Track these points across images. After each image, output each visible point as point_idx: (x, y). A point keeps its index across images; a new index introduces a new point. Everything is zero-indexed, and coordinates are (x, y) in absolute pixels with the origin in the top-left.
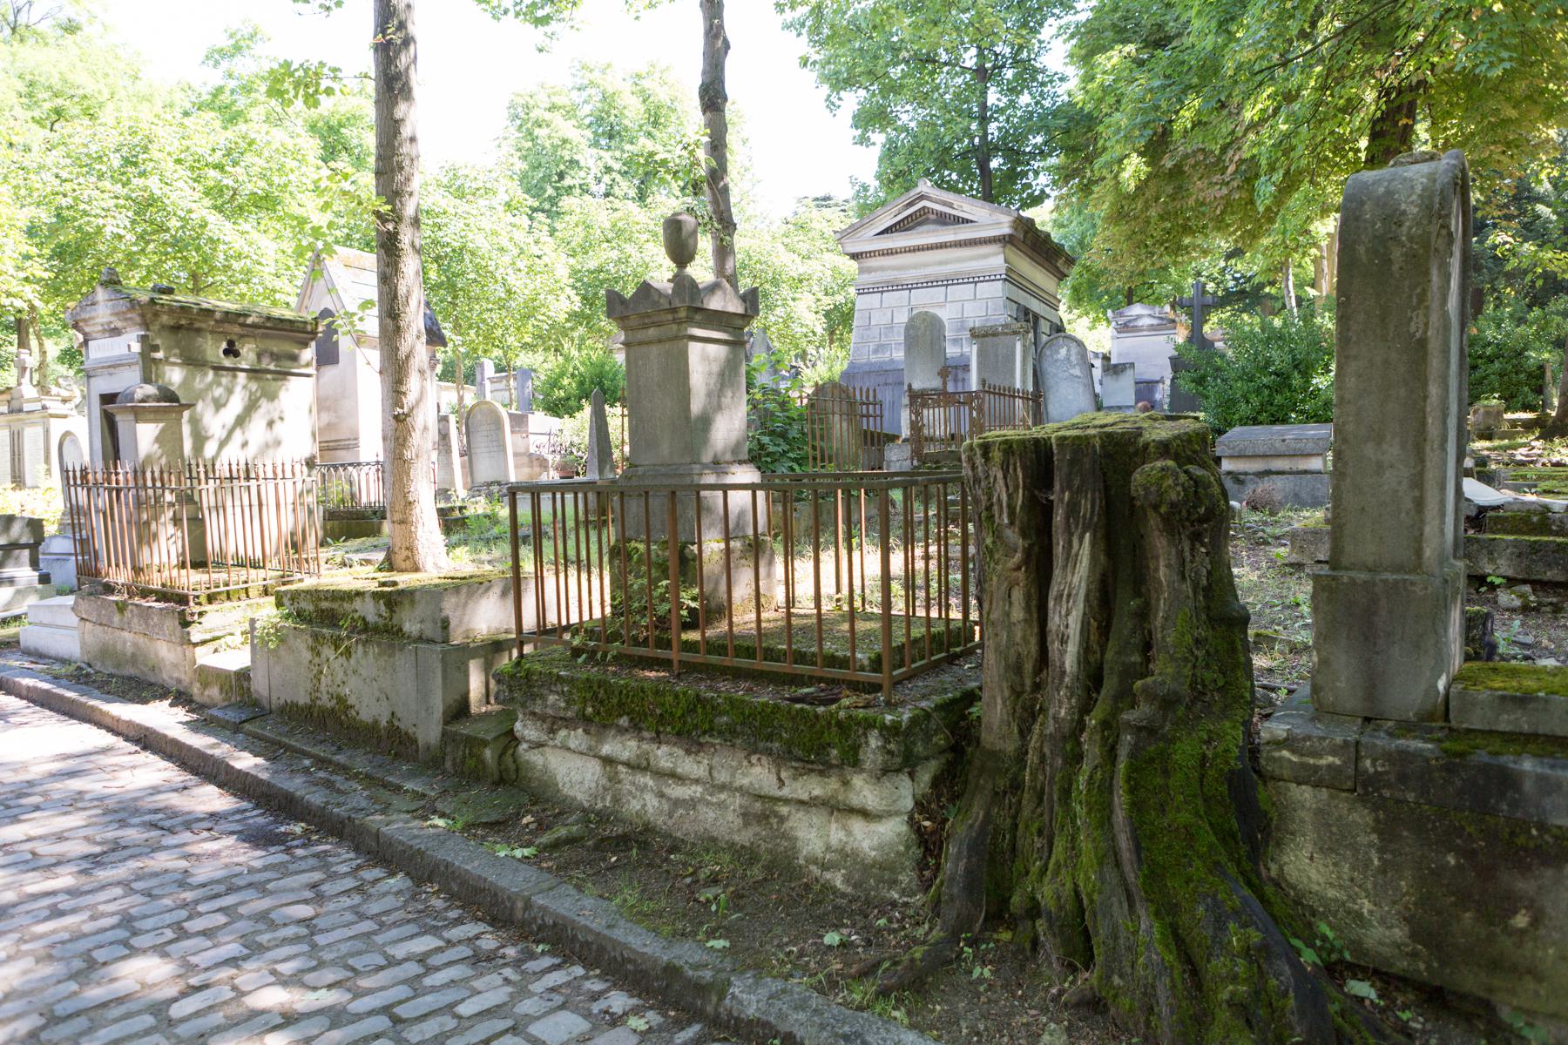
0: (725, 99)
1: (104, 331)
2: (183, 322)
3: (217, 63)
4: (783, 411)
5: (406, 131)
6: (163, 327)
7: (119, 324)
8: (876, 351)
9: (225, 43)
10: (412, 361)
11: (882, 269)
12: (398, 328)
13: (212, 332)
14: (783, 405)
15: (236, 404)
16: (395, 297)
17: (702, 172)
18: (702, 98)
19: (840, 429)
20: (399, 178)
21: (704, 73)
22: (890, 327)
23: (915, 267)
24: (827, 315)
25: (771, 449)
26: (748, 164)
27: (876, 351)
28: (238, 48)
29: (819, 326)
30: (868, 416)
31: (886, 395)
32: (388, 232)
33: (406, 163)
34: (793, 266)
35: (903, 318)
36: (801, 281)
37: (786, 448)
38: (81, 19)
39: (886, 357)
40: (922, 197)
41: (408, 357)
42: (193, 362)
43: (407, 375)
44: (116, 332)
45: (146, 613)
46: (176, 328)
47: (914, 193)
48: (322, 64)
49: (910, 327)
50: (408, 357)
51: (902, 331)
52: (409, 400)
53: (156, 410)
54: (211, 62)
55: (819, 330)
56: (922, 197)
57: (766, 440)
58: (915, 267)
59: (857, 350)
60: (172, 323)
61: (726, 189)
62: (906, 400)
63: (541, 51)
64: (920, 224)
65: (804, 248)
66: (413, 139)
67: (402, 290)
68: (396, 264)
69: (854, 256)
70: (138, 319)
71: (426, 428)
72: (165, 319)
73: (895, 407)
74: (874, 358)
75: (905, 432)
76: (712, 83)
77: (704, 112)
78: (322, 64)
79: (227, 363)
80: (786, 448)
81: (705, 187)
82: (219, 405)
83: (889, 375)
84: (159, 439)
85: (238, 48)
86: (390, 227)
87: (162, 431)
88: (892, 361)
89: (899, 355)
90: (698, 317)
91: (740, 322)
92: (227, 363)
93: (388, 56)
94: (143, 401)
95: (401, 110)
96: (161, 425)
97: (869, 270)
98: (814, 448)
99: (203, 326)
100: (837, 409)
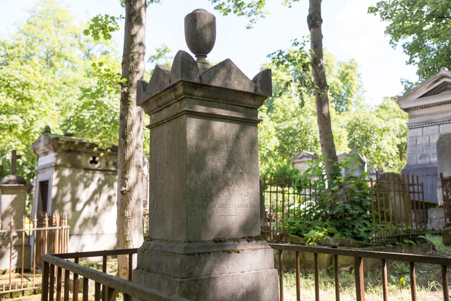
0: (321, 21)
1: (43, 153)
2: (72, 148)
3: (153, 61)
4: (359, 189)
5: (137, 40)
6: (63, 151)
7: (47, 150)
8: (421, 158)
9: (156, 54)
10: (132, 161)
11: (422, 115)
12: (126, 143)
13: (86, 153)
14: (360, 186)
15: (93, 186)
16: (126, 126)
17: (308, 60)
18: (308, 22)
19: (396, 201)
20: (132, 64)
21: (310, 10)
22: (429, 145)
23: (442, 113)
24: (398, 146)
25: (351, 212)
26: (360, 84)
27: (421, 158)
28: (160, 55)
29: (395, 151)
30: (414, 192)
31: (428, 182)
32: (124, 92)
33: (136, 57)
34: (380, 124)
35: (435, 140)
36: (384, 131)
37: (362, 211)
38: (109, 50)
39: (427, 161)
40: (443, 77)
41: (130, 159)
42: (76, 166)
43: (129, 169)
44: (46, 153)
45: (172, 256)
46: (69, 151)
47: (438, 75)
48: (107, 16)
49: (439, 143)
50: (130, 159)
51: (435, 147)
52: (130, 182)
53: (12, 188)
54: (151, 61)
55: (394, 154)
56: (443, 77)
57: (348, 206)
58: (442, 113)
59: (410, 158)
60: (67, 149)
61: (322, 67)
62: (439, 184)
63: (248, 28)
64: (443, 91)
65: (386, 116)
66: (141, 44)
67: (129, 123)
68: (127, 109)
69: (406, 110)
70: (52, 147)
71: (139, 200)
72: (63, 147)
73: (433, 188)
74: (419, 162)
75: (440, 202)
76: (314, 13)
77: (310, 29)
78: (107, 16)
79: (91, 166)
80: (362, 211)
81: (310, 67)
82: (86, 186)
83: (429, 170)
84: (13, 204)
85: (160, 55)
86: (125, 90)
87: (15, 199)
88: (430, 163)
89: (434, 159)
90: (198, 93)
91: (251, 102)
92: (91, 166)
93: (131, 5)
94: (7, 183)
95: (136, 29)
96: (14, 196)
97: (415, 117)
98: (382, 212)
99: (81, 150)
100: (392, 188)
